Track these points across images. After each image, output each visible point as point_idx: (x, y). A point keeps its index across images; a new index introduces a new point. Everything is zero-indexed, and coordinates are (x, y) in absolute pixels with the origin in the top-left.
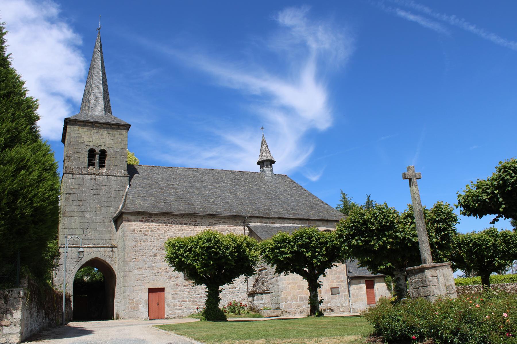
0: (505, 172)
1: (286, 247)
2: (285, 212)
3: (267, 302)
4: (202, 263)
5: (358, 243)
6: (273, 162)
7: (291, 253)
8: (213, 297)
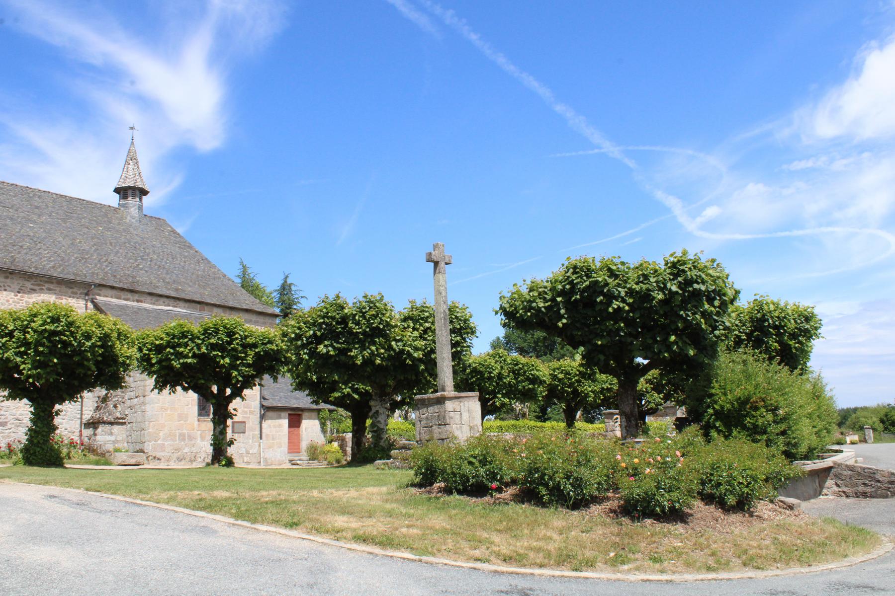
0: (574, 273)
1: (186, 345)
2: (161, 284)
3: (119, 438)
4: (34, 361)
5: (328, 351)
6: (143, 192)
7: (195, 356)
8: (43, 422)
